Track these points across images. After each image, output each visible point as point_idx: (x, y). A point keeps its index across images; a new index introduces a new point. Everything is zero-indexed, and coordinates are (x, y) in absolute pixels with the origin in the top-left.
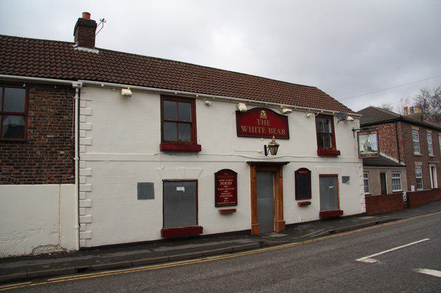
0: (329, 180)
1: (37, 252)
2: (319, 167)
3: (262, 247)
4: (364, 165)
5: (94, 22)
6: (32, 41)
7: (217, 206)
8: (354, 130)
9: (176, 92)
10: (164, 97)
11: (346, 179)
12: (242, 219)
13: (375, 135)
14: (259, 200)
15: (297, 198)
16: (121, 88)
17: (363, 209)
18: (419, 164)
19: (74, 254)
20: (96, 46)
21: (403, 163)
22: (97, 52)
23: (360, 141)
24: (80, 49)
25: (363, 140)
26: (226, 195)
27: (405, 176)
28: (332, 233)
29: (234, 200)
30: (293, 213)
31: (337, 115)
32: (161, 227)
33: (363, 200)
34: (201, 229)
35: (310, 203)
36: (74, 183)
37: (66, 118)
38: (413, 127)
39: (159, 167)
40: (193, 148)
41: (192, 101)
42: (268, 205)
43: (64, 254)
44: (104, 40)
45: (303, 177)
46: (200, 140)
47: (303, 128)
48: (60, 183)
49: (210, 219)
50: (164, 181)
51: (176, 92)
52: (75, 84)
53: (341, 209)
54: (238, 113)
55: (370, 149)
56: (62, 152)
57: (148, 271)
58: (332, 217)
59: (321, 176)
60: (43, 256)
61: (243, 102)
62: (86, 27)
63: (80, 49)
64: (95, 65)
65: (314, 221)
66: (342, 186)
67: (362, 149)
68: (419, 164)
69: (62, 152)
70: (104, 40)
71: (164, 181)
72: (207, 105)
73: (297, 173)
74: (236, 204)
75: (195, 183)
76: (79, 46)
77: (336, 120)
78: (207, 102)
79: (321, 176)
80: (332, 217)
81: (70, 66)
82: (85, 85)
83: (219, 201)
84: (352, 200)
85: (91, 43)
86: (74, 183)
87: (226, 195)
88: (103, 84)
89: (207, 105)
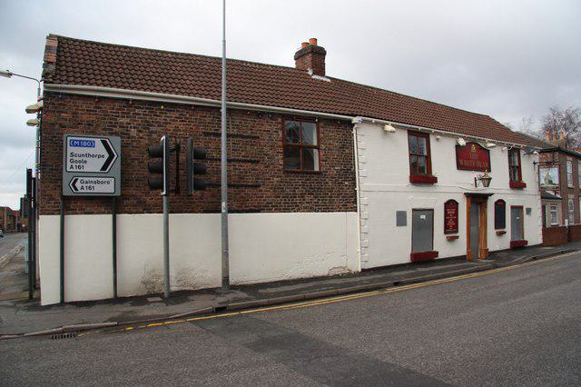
0: (517, 210)
1: (332, 274)
2: (512, 199)
3: (494, 268)
4: (542, 198)
5: (322, 49)
6: (77, 43)
7: (445, 233)
8: (535, 163)
9: (420, 128)
10: (411, 132)
11: (529, 211)
12: (460, 248)
13: (557, 169)
14: (472, 228)
15: (496, 228)
16: (384, 124)
17: (540, 241)
18: (571, 196)
19: (357, 274)
20: (327, 74)
21: (558, 196)
22: (329, 80)
23: (542, 174)
24: (314, 77)
25: (544, 173)
26: (451, 223)
27: (560, 209)
28: (535, 259)
29: (456, 228)
30: (496, 243)
31: (525, 149)
32: (409, 251)
33: (540, 231)
34: (436, 254)
35: (457, 237)
36: (356, 211)
37: (347, 151)
38: (568, 158)
39: (411, 196)
40: (432, 181)
41: (426, 135)
42: (476, 237)
43: (350, 275)
44: (335, 68)
45: (500, 205)
46: (435, 172)
47: (499, 159)
48: (346, 211)
49: (443, 247)
50: (413, 210)
51: (420, 128)
52: (355, 120)
53: (526, 239)
54: (458, 147)
55: (550, 182)
56: (346, 183)
57: (450, 282)
58: (519, 246)
59: (512, 207)
60: (337, 277)
61: (463, 137)
62: (313, 54)
63: (314, 77)
64: (107, 64)
65: (76, 302)
66: (526, 216)
67: (543, 181)
68: (571, 196)
69: (346, 183)
70: (335, 68)
71: (413, 210)
72: (438, 139)
73: (496, 203)
74: (457, 232)
75: (431, 212)
76: (314, 74)
77: (522, 153)
78: (438, 137)
79: (512, 207)
80: (519, 246)
81: (78, 70)
82: (364, 121)
83: (446, 227)
84: (533, 234)
85: (320, 69)
86: (356, 211)
87: (451, 223)
88: (374, 120)
89: (438, 139)
